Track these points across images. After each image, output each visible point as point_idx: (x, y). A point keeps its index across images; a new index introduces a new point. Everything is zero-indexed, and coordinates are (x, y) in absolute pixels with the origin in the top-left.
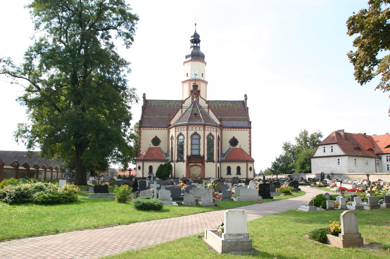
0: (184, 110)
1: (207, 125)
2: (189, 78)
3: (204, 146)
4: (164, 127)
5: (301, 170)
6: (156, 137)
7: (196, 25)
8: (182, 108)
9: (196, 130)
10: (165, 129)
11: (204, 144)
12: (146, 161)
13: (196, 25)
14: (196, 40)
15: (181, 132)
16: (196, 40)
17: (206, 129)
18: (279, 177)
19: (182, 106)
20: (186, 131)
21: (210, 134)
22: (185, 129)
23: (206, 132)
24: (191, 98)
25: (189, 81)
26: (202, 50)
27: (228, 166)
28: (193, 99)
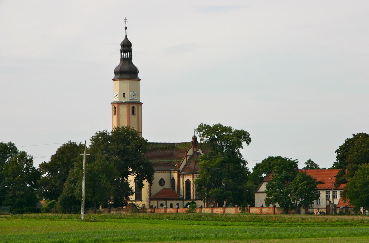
0: (188, 158)
1: (195, 174)
2: (127, 99)
3: (183, 185)
4: (167, 171)
5: (243, 211)
6: (10, 142)
7: (126, 28)
8: (187, 157)
9: (188, 178)
10: (168, 172)
11: (193, 192)
12: (168, 200)
13: (126, 28)
14: (126, 47)
15: (188, 179)
16: (126, 47)
17: (185, 177)
18: (126, 214)
19: (186, 155)
20: (192, 179)
21: (188, 180)
22: (191, 176)
23: (184, 179)
24: (192, 148)
25: (128, 105)
26: (135, 62)
27: (171, 203)
28: (193, 149)
